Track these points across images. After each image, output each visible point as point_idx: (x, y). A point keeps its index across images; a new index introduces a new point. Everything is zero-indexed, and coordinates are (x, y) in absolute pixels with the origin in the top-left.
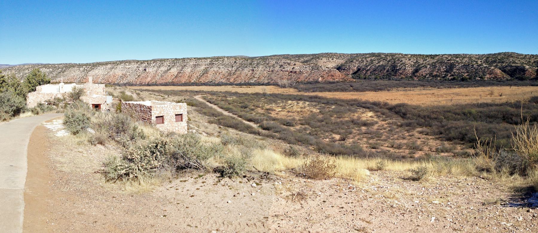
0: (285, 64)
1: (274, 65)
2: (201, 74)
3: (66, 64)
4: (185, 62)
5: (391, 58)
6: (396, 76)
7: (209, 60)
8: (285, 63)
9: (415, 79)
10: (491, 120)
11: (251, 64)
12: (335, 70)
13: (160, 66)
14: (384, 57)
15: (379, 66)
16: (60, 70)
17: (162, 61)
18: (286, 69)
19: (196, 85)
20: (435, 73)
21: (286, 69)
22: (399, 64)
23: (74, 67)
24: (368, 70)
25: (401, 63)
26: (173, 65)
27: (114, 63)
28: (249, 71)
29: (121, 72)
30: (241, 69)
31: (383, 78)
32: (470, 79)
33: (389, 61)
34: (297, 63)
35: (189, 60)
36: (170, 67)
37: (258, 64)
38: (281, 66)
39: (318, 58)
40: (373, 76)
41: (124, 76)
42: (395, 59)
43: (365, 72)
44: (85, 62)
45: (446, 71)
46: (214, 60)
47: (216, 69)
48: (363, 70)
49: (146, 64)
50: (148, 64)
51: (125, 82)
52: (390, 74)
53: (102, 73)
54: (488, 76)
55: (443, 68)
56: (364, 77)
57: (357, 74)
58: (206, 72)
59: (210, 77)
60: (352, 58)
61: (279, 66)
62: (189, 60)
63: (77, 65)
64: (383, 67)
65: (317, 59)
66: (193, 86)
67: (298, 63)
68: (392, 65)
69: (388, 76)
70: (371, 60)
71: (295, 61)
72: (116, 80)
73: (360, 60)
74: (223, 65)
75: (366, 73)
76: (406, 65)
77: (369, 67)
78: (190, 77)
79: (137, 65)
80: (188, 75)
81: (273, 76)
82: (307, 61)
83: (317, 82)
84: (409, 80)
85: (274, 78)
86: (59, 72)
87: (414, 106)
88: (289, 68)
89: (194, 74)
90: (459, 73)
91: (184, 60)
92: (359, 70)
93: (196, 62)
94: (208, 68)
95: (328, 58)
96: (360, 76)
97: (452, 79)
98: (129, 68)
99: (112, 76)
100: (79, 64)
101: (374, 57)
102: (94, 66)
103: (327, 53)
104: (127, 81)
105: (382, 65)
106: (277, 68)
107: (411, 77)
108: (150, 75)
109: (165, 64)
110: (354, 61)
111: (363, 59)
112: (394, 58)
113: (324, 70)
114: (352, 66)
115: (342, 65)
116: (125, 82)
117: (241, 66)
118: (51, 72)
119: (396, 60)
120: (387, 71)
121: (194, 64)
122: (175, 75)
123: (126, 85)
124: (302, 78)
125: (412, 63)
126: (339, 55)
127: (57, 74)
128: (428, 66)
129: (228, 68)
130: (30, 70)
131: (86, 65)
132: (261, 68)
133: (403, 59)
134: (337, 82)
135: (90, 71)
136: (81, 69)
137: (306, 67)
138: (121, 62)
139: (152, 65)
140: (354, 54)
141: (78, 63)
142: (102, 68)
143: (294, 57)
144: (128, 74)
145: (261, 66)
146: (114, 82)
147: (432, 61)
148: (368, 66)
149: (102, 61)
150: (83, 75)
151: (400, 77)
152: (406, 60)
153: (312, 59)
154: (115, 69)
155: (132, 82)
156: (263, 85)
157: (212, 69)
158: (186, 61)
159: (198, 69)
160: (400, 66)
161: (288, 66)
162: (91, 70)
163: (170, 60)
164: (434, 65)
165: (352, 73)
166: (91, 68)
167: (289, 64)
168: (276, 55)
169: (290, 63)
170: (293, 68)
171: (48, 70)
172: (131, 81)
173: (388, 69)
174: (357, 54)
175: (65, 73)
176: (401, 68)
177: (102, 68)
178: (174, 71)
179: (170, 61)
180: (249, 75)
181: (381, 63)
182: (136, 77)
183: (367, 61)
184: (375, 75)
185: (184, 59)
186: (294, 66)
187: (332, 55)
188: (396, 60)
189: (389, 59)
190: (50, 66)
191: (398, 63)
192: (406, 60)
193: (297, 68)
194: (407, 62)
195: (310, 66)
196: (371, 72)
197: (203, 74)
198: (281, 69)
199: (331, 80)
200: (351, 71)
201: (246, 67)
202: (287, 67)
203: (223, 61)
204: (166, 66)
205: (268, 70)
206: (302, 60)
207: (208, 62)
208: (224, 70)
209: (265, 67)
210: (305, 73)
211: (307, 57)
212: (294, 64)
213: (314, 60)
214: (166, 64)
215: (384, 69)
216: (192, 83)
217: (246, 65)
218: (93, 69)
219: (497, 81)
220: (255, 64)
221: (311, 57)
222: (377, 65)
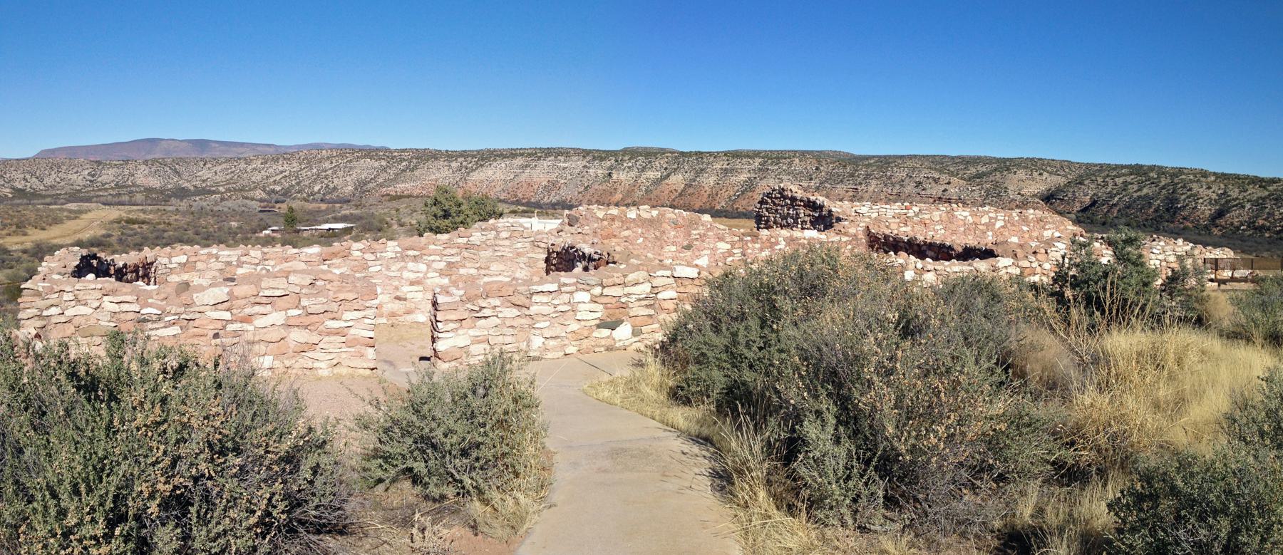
0: (928, 181)
1: (903, 181)
2: (738, 191)
3: (417, 150)
4: (703, 163)
5: (1168, 180)
6: (1172, 222)
7: (758, 160)
8: (928, 178)
11: (852, 175)
12: (1037, 200)
13: (643, 169)
14: (1156, 176)
15: (1139, 197)
16: (404, 164)
17: (650, 154)
18: (928, 192)
19: (726, 217)
21: (929, 191)
22: (1183, 197)
23: (436, 159)
24: (1115, 205)
25: (1189, 193)
26: (676, 166)
27: (530, 155)
28: (847, 192)
29: (546, 176)
30: (829, 186)
31: (1144, 225)
33: (1163, 188)
34: (954, 180)
35: (712, 159)
36: (668, 171)
37: (868, 176)
38: (919, 184)
39: (1008, 169)
41: (553, 185)
42: (1178, 183)
43: (1105, 210)
44: (459, 147)
46: (770, 161)
48: (1104, 205)
49: (613, 161)
50: (616, 161)
51: (554, 201)
52: (1161, 217)
53: (502, 177)
56: (1103, 220)
57: (1089, 213)
58: (750, 186)
60: (1091, 172)
61: (915, 185)
62: (712, 159)
63: (442, 154)
64: (1148, 200)
65: (1005, 173)
66: (720, 217)
67: (957, 180)
68: (1167, 198)
70: (1125, 183)
71: (952, 174)
72: (533, 194)
73: (1100, 180)
74: (789, 174)
75: (1108, 211)
76: (1198, 199)
77: (1116, 199)
79: (584, 163)
80: (708, 193)
82: (980, 176)
84: (1199, 234)
86: (403, 170)
89: (724, 190)
91: (702, 158)
92: (1094, 203)
93: (728, 164)
94: (755, 178)
95: (1031, 171)
96: (1095, 218)
98: (564, 169)
99: (525, 186)
100: (447, 151)
101: (1133, 177)
102: (483, 159)
103: (1032, 159)
104: (557, 198)
105: (1146, 196)
107: (1206, 227)
108: (620, 189)
109: (657, 163)
110: (1086, 182)
111: (1107, 180)
112: (1176, 180)
113: (1013, 200)
114: (1079, 194)
115: (1059, 190)
116: (554, 199)
117: (830, 179)
118: (384, 169)
119: (1179, 186)
120: (1156, 211)
121: (724, 167)
122: (679, 191)
123: (557, 207)
126: (1058, 165)
127: (397, 175)
129: (801, 181)
130: (334, 161)
131: (464, 154)
132: (873, 186)
133: (1195, 186)
135: (473, 170)
136: (454, 165)
137: (972, 191)
138: (548, 152)
139: (625, 165)
140: (1096, 165)
141: (443, 149)
142: (502, 164)
143: (956, 163)
144: (562, 181)
145: (874, 182)
146: (529, 199)
148: (1115, 196)
149: (501, 147)
150: (458, 179)
151: (1182, 226)
152: (1202, 187)
153: (996, 170)
154: (532, 169)
155: (570, 202)
157: (764, 183)
158: (705, 160)
160: (1185, 200)
161: (933, 184)
162: (476, 169)
163: (669, 155)
165: (1079, 209)
166: (477, 163)
167: (936, 181)
168: (915, 156)
169: (939, 178)
170: (943, 191)
171: (376, 164)
172: (569, 199)
173: (1159, 205)
174: (1101, 166)
175: (416, 173)
176: (1187, 205)
177: (503, 165)
178: (677, 181)
179: (667, 157)
181: (1145, 191)
182: (580, 190)
183: (1116, 185)
184: (1127, 216)
185: (699, 155)
186: (947, 187)
187: (1043, 165)
188: (1179, 186)
189: (1163, 183)
190: (381, 153)
191: (1182, 194)
192: (1202, 187)
194: (1203, 191)
195: (982, 188)
196: (1119, 211)
197: (743, 192)
198: (918, 190)
200: (1078, 205)
201: (842, 181)
202: (931, 188)
203: (790, 164)
204: (658, 168)
205: (890, 191)
206: (973, 170)
207: (757, 164)
209: (882, 185)
210: (969, 202)
211: (985, 164)
212: (947, 181)
213: (998, 173)
214: (658, 165)
216: (717, 210)
217: (841, 178)
218: (481, 165)
220: (862, 177)
221: (994, 166)
222: (1135, 195)
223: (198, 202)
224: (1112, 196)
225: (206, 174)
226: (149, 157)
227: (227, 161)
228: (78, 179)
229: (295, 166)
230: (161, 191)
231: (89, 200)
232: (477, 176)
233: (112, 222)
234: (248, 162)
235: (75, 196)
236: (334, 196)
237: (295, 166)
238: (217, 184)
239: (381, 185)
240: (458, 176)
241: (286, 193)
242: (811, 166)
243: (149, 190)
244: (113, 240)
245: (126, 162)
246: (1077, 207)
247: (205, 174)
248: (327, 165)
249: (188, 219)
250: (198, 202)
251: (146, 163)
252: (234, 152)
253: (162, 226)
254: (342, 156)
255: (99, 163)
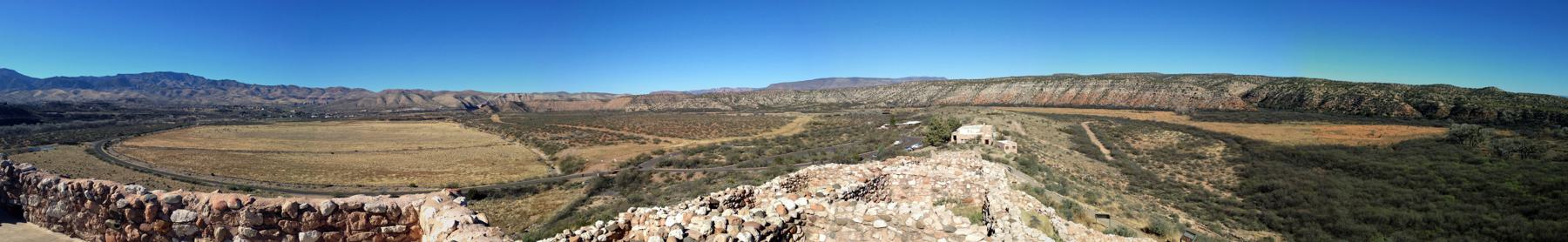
9: (1320, 111)
10: (917, 159)
11: (1153, 87)
20: (1342, 106)
27: (1008, 81)
32: (1376, 114)
34: (1199, 88)
40: (1278, 106)
41: (1019, 95)
45: (1354, 105)
47: (1116, 91)
54: (1396, 112)
55: (1351, 101)
58: (1106, 93)
59: (1110, 99)
64: (1291, 96)
69: (1293, 107)
70: (1282, 87)
78: (1089, 99)
81: (1173, 101)
83: (1216, 110)
85: (1175, 103)
87: (1353, 144)
88: (1191, 94)
90: (1367, 108)
92: (1267, 98)
97: (1357, 114)
106: (1179, 93)
114: (1261, 94)
124: (1203, 105)
125: (1322, 94)
128: (1336, 98)
134: (1238, 111)
147: (1341, 91)
156: (1162, 110)
157: (1112, 92)
159: (1098, 90)
164: (1342, 98)
167: (1192, 89)
178: (1073, 92)
180: (1150, 99)
181: (1290, 91)
193: (1199, 94)
199: (1232, 108)
208: (1124, 92)
215: (1292, 98)
219: (1405, 120)
223: (854, 111)
224: (1275, 94)
225: (859, 96)
226: (822, 88)
227: (867, 89)
228: (789, 99)
229: (899, 90)
230: (837, 104)
231: (794, 110)
232: (984, 92)
233: (807, 124)
234: (877, 89)
235: (788, 108)
236: (918, 104)
237: (899, 90)
238: (863, 100)
239: (939, 98)
240: (976, 92)
241: (895, 104)
242: (1134, 83)
243: (823, 105)
244: (808, 134)
245: (811, 91)
246: (1260, 99)
247: (857, 95)
248: (914, 89)
249: (849, 120)
250: (854, 111)
251: (821, 91)
252: (871, 84)
253: (829, 126)
254: (921, 84)
255: (799, 92)
